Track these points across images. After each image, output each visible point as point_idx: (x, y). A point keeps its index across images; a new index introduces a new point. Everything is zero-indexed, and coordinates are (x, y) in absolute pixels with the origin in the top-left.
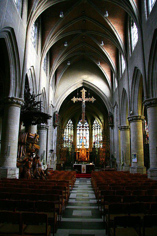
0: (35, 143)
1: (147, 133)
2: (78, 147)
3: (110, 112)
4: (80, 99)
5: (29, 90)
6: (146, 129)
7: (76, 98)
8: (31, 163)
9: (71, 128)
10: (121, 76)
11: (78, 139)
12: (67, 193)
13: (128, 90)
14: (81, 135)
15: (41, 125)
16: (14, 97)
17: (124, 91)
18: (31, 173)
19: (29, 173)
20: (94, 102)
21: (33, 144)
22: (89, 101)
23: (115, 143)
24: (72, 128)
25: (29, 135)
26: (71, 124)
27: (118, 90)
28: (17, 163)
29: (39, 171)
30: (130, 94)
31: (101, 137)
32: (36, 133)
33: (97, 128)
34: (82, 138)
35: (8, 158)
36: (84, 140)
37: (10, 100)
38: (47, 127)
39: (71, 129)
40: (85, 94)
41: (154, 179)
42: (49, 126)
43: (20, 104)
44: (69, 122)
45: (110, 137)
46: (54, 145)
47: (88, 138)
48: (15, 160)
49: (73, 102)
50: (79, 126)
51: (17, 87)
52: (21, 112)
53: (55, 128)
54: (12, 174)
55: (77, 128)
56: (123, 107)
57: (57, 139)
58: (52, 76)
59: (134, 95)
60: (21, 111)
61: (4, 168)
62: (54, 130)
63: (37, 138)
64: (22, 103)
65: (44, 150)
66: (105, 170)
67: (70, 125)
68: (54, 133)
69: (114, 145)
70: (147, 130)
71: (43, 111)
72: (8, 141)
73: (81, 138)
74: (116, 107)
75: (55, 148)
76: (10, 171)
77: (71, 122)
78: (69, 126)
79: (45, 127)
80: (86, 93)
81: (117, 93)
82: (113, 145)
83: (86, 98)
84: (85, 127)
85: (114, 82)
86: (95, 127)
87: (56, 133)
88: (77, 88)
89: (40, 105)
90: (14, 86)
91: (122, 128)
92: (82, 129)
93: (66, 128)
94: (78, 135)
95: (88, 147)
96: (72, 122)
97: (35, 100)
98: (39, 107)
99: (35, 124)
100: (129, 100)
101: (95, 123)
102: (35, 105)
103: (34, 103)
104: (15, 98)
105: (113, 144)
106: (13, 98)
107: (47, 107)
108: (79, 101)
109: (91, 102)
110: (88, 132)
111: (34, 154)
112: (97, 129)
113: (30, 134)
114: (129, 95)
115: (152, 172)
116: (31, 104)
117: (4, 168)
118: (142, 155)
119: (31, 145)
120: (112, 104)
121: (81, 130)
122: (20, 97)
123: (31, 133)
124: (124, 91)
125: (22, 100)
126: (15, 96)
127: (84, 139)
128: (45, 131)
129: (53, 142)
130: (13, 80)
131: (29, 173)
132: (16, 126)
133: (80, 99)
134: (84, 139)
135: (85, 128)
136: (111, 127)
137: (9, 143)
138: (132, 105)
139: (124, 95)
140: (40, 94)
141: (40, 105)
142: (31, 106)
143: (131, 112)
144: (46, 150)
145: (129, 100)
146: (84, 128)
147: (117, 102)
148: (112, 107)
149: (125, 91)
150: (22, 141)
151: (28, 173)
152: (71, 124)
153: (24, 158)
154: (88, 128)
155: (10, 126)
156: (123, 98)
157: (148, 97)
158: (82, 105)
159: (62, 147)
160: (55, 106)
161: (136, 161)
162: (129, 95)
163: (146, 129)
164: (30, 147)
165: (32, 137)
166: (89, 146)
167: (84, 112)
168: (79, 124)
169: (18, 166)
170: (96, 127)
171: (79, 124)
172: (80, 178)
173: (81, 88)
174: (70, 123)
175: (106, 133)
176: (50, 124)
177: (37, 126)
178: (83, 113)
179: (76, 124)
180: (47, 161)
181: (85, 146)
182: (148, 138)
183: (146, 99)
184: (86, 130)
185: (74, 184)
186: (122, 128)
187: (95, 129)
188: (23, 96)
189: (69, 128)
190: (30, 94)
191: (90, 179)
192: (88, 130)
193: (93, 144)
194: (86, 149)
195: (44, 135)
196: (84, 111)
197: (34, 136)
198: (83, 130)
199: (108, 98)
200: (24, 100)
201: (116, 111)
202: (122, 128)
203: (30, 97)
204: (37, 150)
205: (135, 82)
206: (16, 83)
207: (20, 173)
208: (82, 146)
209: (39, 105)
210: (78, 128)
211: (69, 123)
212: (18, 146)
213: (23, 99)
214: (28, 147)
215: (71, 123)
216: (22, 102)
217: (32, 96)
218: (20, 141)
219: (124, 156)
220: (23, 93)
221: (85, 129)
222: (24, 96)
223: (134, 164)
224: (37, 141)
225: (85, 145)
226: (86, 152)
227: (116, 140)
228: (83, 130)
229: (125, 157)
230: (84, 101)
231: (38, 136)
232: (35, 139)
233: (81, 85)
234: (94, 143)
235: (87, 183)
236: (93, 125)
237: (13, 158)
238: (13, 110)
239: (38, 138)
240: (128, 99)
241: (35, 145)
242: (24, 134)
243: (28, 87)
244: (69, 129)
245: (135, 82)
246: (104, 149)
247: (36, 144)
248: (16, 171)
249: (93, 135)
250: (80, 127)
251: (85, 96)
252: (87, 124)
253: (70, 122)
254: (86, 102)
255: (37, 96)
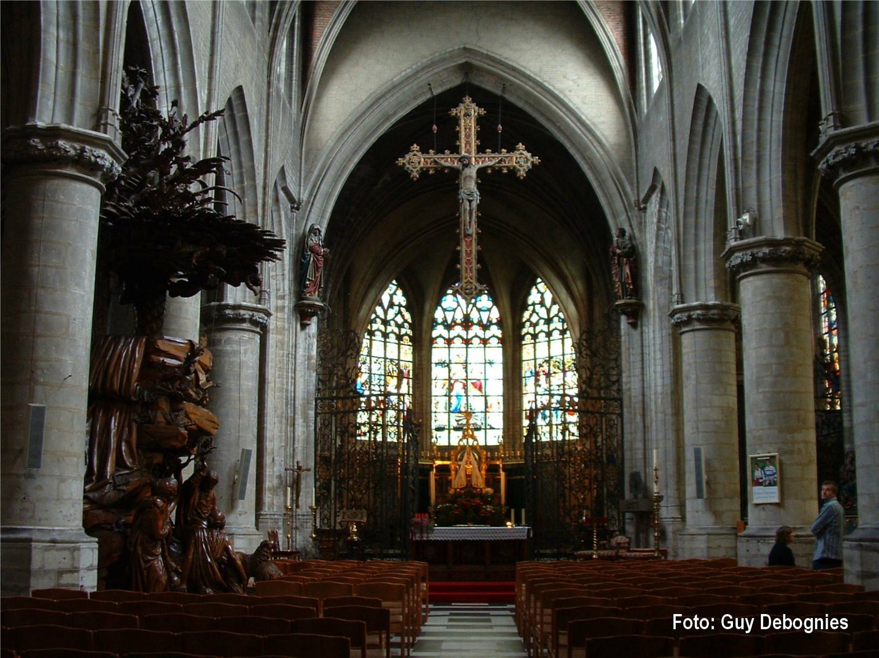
0: (189, 399)
1: (832, 352)
2: (441, 439)
3: (622, 232)
4: (448, 160)
5: (150, 94)
6: (824, 325)
7: (424, 150)
8: (164, 512)
9: (396, 330)
10: (682, 22)
11: (438, 389)
12: (376, 450)
13: (726, 90)
14: (458, 372)
15: (227, 306)
16: (64, 126)
17: (705, 102)
18: (166, 565)
19: (159, 564)
20: (529, 172)
21: (175, 401)
22: (500, 169)
23: (653, 407)
24: (403, 331)
25: (152, 349)
26: (396, 308)
27: (665, 101)
28: (85, 513)
29: (212, 553)
30: (739, 114)
31: (572, 378)
32: (196, 340)
33: (545, 328)
34: (465, 387)
35: (30, 476)
36: (470, 399)
37: (36, 142)
38: (258, 316)
39: (399, 337)
40: (463, 266)
41: (873, 585)
42: (272, 311)
43: (93, 167)
44: (385, 298)
45: (619, 374)
46: (299, 421)
47: (496, 388)
48: (76, 488)
49: (406, 174)
50: (445, 320)
51: (81, 71)
52: (106, 219)
53: (304, 326)
54: (55, 566)
55: (435, 334)
56: (698, 198)
57: (318, 390)
58: (287, 26)
59: (760, 119)
60: (103, 211)
61: (12, 536)
62: (301, 335)
63: (198, 366)
64: (107, 160)
65: (242, 446)
66: (600, 557)
67: (391, 313)
68: (301, 352)
69: (644, 416)
70: (830, 332)
71: (233, 209)
72: (32, 381)
73: (458, 389)
74: (655, 198)
75: (308, 437)
76: (46, 549)
77: (400, 298)
78: (385, 322)
79: (247, 314)
80: (480, 120)
81: (663, 119)
82: (639, 419)
83: (481, 149)
84: (480, 323)
85: (642, 41)
86: (534, 325)
87: (314, 353)
88: (429, 96)
89: (219, 180)
90: (61, 64)
91: (695, 314)
92: (463, 334)
93: (371, 333)
94: (438, 373)
95: (494, 438)
96: (404, 295)
97: (187, 147)
98: (211, 194)
99: (187, 291)
100: (735, 147)
101: (534, 304)
102: (186, 176)
103: (181, 168)
104: (68, 131)
105: (639, 411)
106: (53, 133)
107: (260, 201)
108: (445, 167)
109: (513, 172)
110: (496, 353)
111: (184, 459)
112: (549, 334)
113: (161, 344)
114: (733, 123)
115: (868, 548)
116: (164, 172)
117: (12, 536)
118: (810, 462)
119: (164, 405)
120: (631, 184)
121: (458, 342)
122: (96, 128)
123: (162, 338)
124: (705, 102)
125: (105, 144)
126: (69, 117)
127: (472, 391)
128: (247, 335)
129: (299, 402)
130: (53, 30)
131: (159, 564)
132: (78, 291)
133: (448, 160)
134: (472, 391)
135: (476, 330)
136: (629, 316)
137: (39, 390)
138: (752, 181)
139: (699, 129)
140: (213, 110)
141: (219, 180)
142: (161, 182)
143: (746, 217)
144: (253, 447)
145: (735, 147)
146: (471, 334)
147: (661, 170)
148: (633, 199)
149: (710, 100)
150: (116, 386)
151: (152, 569)
152: (396, 308)
153: (127, 484)
154: (499, 333)
155: (41, 292)
156: (697, 147)
157: (843, 119)
158: (463, 194)
159: (349, 429)
160: (304, 197)
161: (776, 500)
162: (733, 123)
163: (825, 330)
164: (160, 418)
165: (168, 361)
166: (500, 433)
167: (473, 229)
168: (444, 310)
169: (90, 527)
170: (542, 327)
171: (444, 310)
172: (455, 605)
173: (453, 97)
174: (391, 305)
175: (601, 351)
176: (280, 303)
177: (200, 297)
178: (467, 236)
179: (427, 307)
180: (266, 510)
181: (483, 431)
182: (837, 378)
183: (832, 132)
184: (485, 341)
185: (417, 633)
186: (689, 317)
187: (535, 336)
188: (115, 121)
189: (389, 329)
190: (157, 115)
191: (509, 606)
192: (494, 342)
193: (526, 423)
194: (486, 448)
195: (243, 358)
196: (474, 226)
197: (183, 355)
198: (467, 342)
199: (607, 152)
200: (118, 143)
201: (659, 221)
202: (689, 317)
203: (160, 131)
204: (205, 438)
205: (766, 55)
206: (74, 44)
207: (105, 566)
208: (460, 433)
209: (211, 179)
210: (439, 331)
211: (386, 304)
212: (92, 414)
213: (114, 134)
214: (150, 422)
215: (400, 305)
216: (107, 156)
217: (167, 126)
218: (104, 383)
219: (705, 477)
220: (115, 104)
221: (481, 333)
222: (121, 122)
223: (763, 514)
224: (197, 385)
225: (479, 429)
226: (484, 466)
227: (659, 389)
228: (467, 342)
229: (708, 483)
230: (472, 172)
231: (206, 358)
232: (189, 373)
233: (456, 81)
234: (533, 415)
235: (491, 627)
236: (526, 315)
237: (62, 480)
238: (57, 202)
239: (207, 370)
240: (727, 144)
241: (189, 406)
242: (126, 344)
243: (148, 77)
244: (385, 335)
245: (768, 43)
246: (574, 502)
247: (199, 403)
248: (82, 551)
249: (527, 368)
250: (449, 327)
251: (474, 142)
252: (489, 310)
253: (391, 296)
254: (481, 172)
255: (195, 125)
